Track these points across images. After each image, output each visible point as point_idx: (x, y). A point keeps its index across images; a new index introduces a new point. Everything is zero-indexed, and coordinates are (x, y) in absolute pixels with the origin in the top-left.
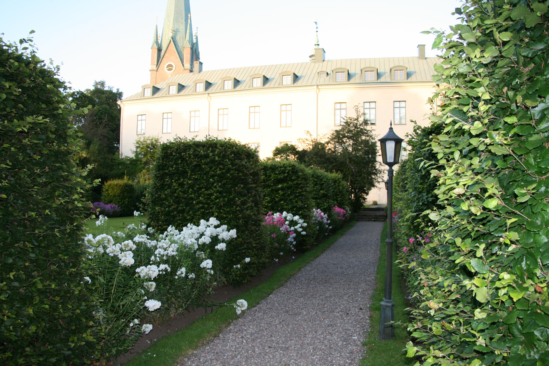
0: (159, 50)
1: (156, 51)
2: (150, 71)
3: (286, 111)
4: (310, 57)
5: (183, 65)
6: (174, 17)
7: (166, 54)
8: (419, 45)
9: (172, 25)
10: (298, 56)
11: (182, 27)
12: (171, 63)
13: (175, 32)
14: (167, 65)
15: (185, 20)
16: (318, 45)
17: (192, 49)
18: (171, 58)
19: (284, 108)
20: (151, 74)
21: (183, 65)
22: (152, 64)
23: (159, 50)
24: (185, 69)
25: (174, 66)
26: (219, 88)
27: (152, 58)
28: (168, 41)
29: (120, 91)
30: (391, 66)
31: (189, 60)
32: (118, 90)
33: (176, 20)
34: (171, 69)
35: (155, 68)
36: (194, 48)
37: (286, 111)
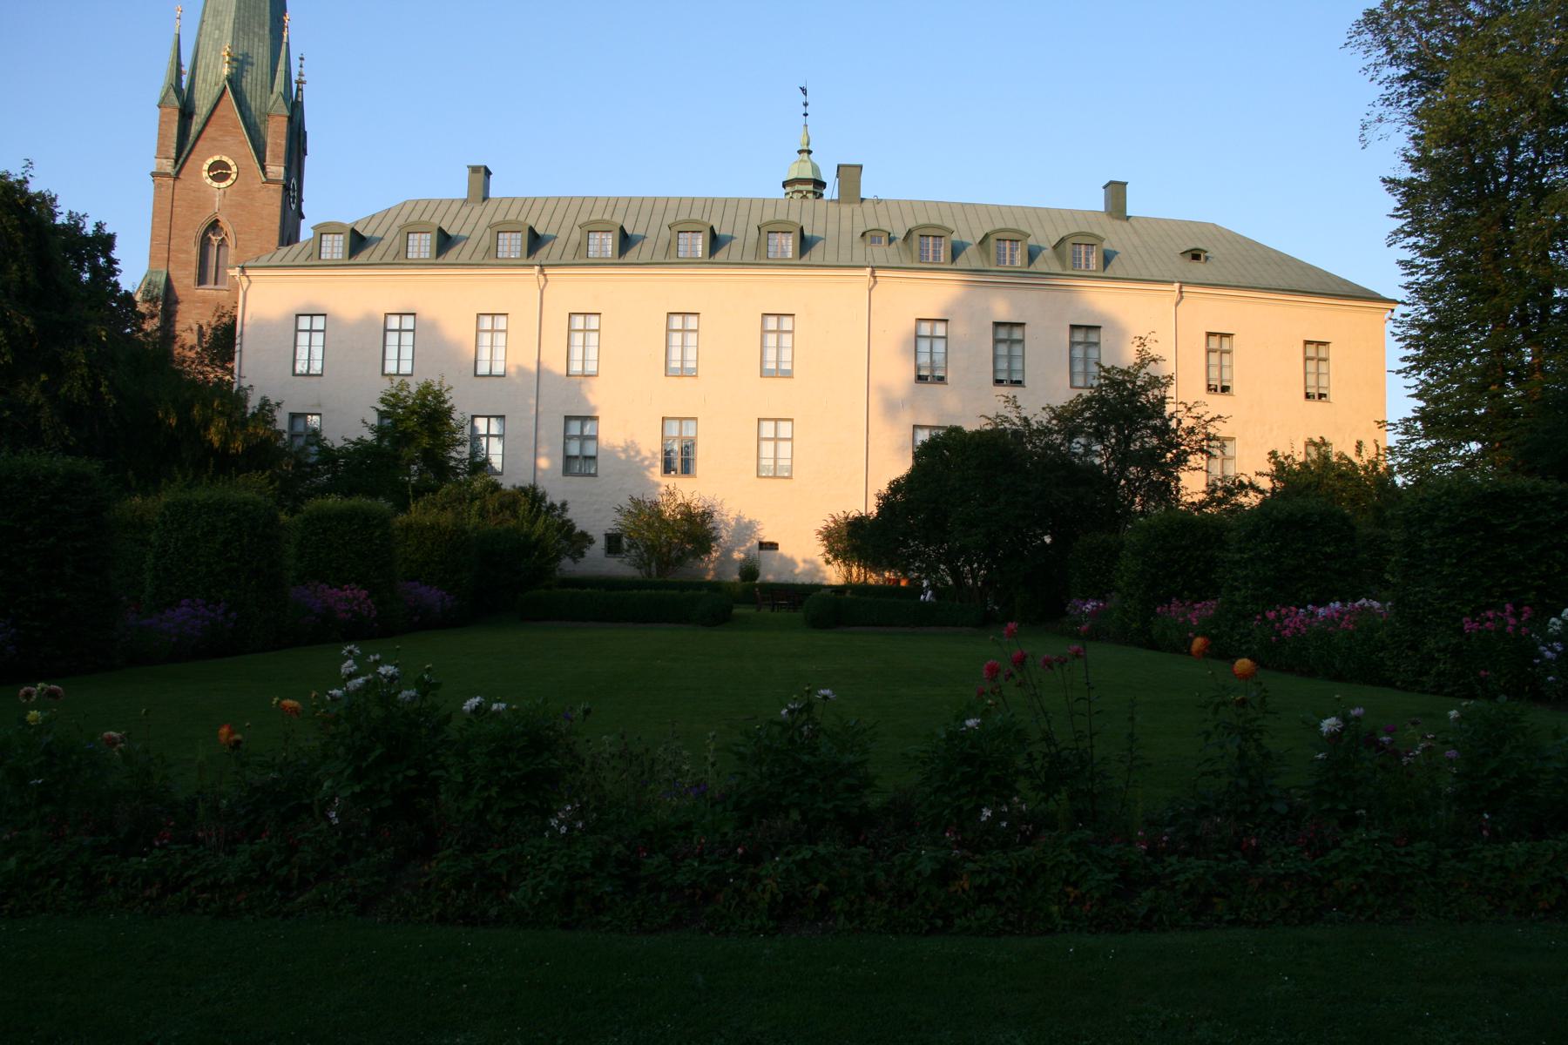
0: (186, 113)
1: (175, 117)
2: (154, 175)
3: (311, 331)
4: (785, 185)
5: (263, 168)
6: (237, 18)
7: (209, 130)
8: (1111, 183)
9: (228, 42)
10: (753, 177)
11: (261, 53)
12: (225, 159)
13: (240, 64)
14: (210, 161)
15: (271, 31)
16: (809, 152)
17: (290, 119)
18: (225, 144)
19: (677, 322)
20: (158, 187)
21: (263, 168)
22: (161, 154)
23: (186, 113)
24: (269, 181)
25: (234, 169)
26: (392, 252)
27: (162, 136)
28: (216, 91)
29: (108, 230)
30: (911, 224)
31: (283, 155)
32: (99, 226)
33: (242, 27)
34: (225, 177)
35: (168, 166)
36: (296, 118)
37: (311, 331)
